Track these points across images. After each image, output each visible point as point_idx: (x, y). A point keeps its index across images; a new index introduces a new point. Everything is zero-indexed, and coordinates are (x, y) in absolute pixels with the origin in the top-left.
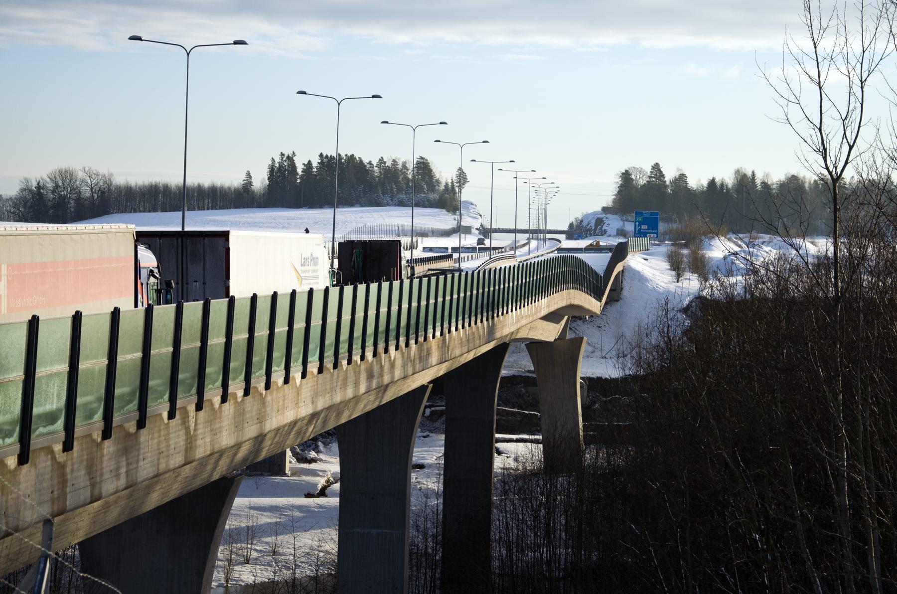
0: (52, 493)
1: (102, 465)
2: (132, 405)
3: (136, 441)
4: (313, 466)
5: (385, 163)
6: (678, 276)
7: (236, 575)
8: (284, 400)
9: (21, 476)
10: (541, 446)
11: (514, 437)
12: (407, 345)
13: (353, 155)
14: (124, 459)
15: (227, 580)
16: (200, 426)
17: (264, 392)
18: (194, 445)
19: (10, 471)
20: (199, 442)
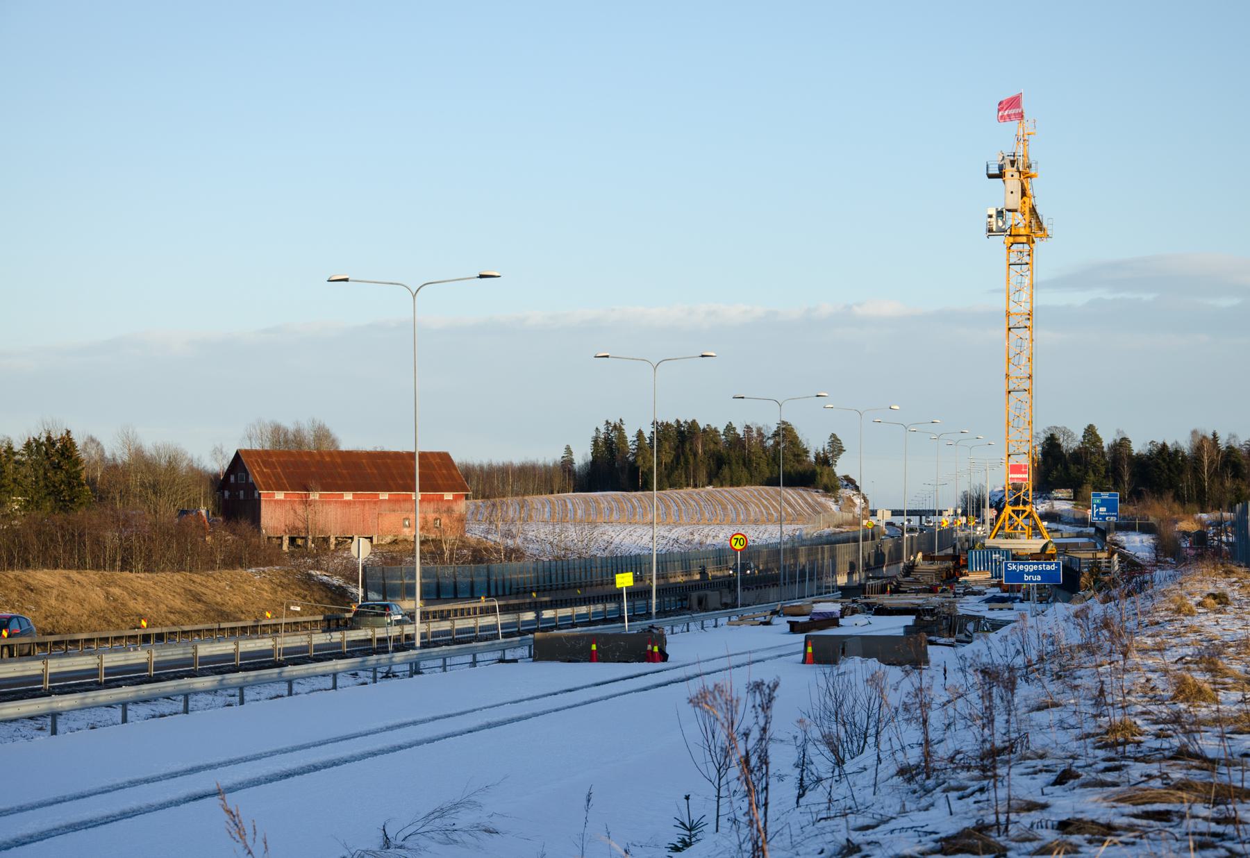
5: (734, 429)
13: (694, 421)
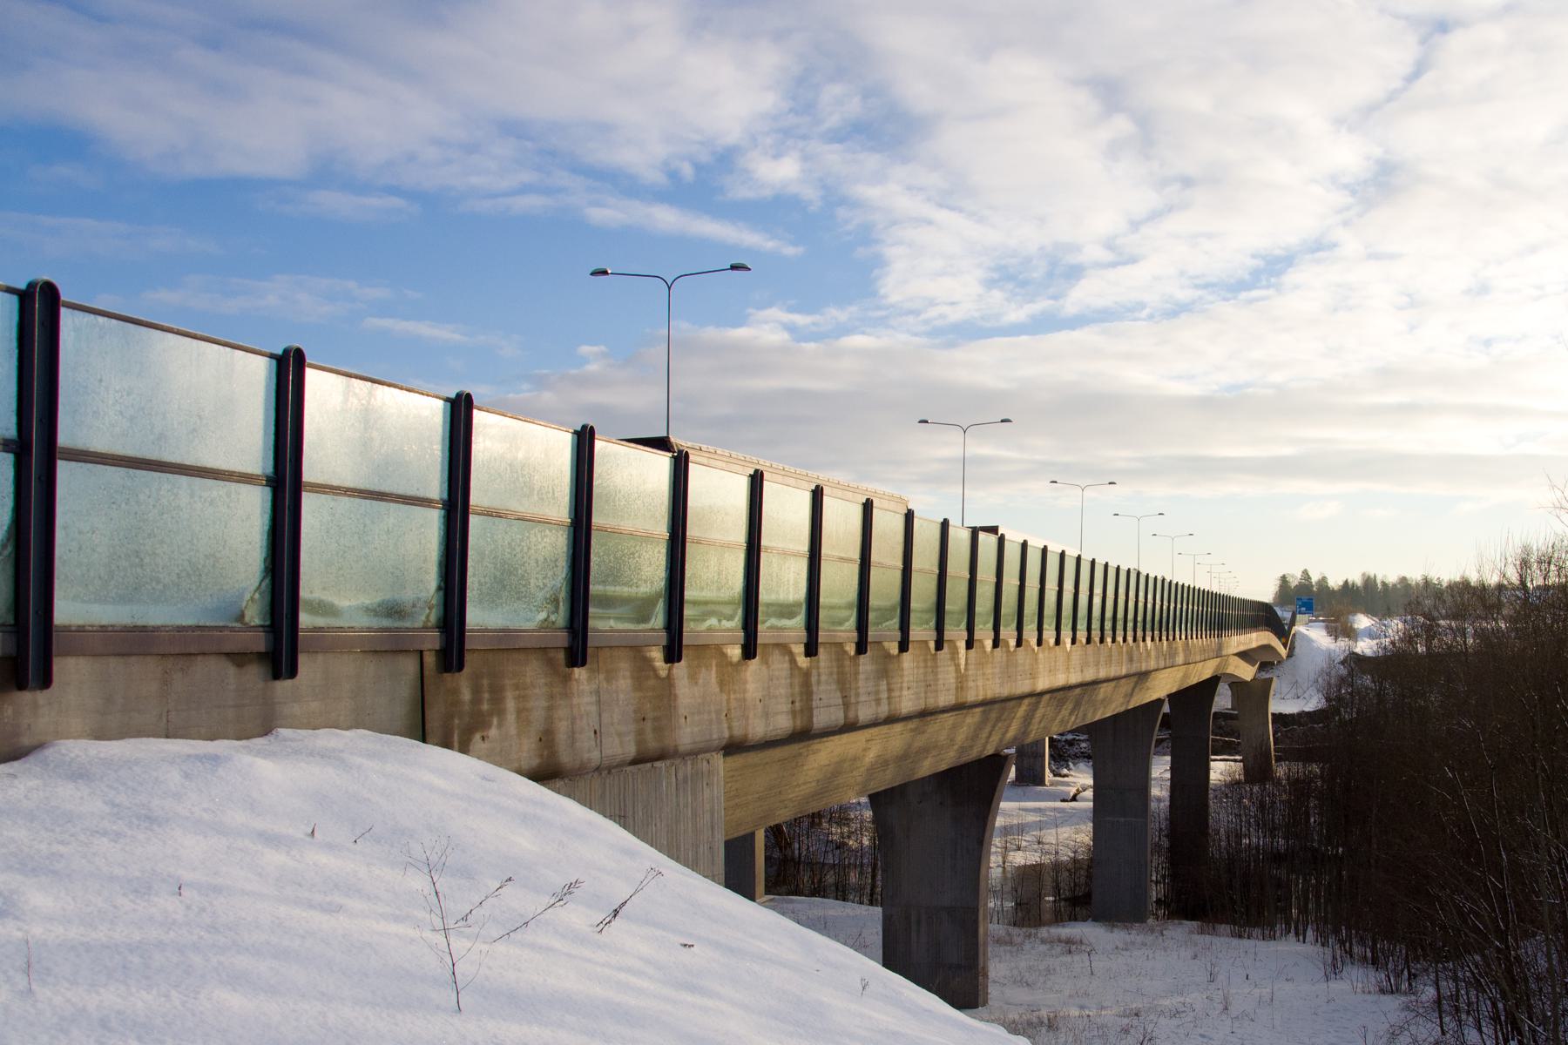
0: (792, 703)
1: (857, 683)
2: (892, 622)
3: (899, 666)
4: (1066, 779)
6: (1336, 640)
7: (1010, 858)
8: (1055, 662)
9: (748, 674)
10: (1242, 764)
11: (1219, 757)
12: (1160, 639)
14: (885, 682)
15: (1004, 863)
16: (971, 667)
17: (1036, 648)
18: (965, 685)
19: (731, 664)
20: (971, 684)
